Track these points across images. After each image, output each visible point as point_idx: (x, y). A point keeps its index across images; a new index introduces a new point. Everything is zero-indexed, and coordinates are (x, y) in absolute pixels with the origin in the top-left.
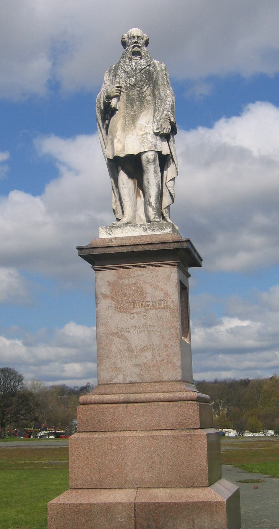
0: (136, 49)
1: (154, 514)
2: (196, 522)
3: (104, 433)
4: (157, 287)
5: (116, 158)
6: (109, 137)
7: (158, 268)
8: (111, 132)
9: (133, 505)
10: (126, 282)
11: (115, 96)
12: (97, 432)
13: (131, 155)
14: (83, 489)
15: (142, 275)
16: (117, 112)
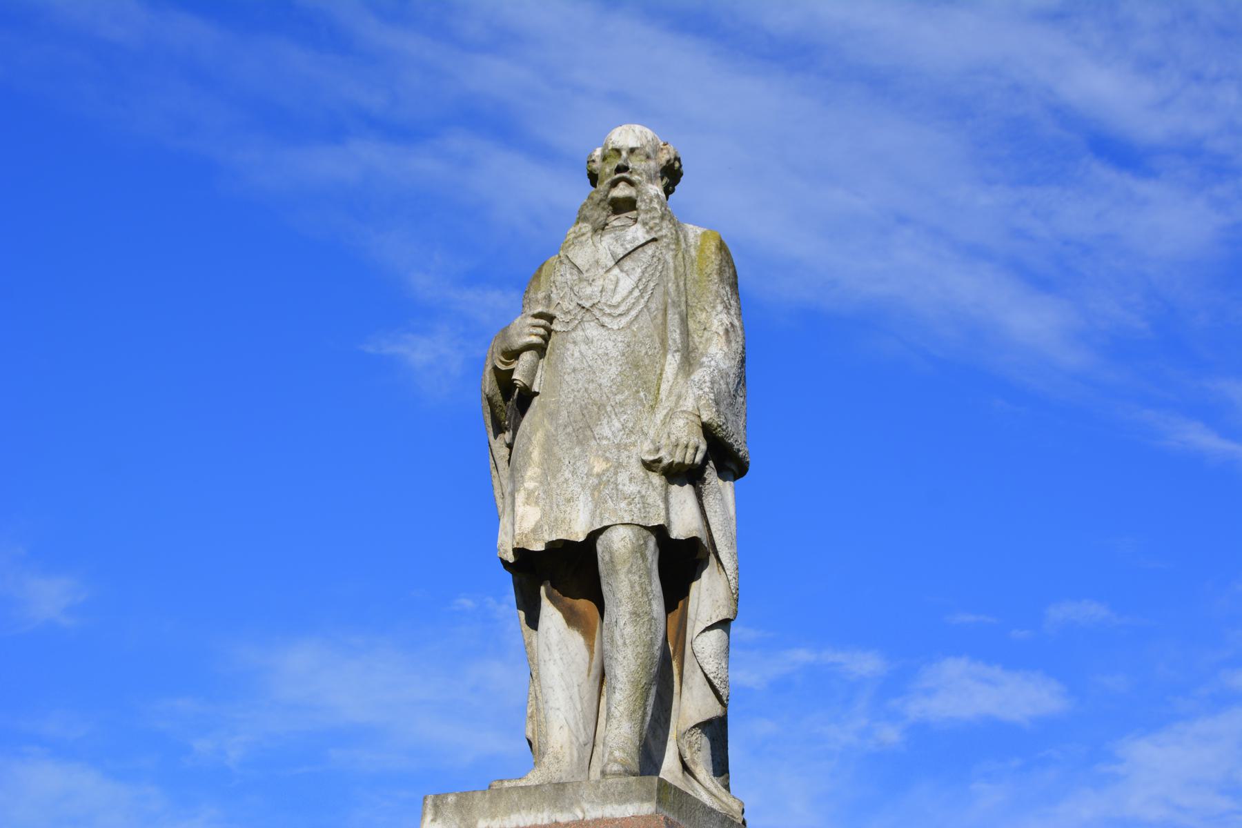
0: (622, 191)
13: (695, 575)
16: (536, 399)
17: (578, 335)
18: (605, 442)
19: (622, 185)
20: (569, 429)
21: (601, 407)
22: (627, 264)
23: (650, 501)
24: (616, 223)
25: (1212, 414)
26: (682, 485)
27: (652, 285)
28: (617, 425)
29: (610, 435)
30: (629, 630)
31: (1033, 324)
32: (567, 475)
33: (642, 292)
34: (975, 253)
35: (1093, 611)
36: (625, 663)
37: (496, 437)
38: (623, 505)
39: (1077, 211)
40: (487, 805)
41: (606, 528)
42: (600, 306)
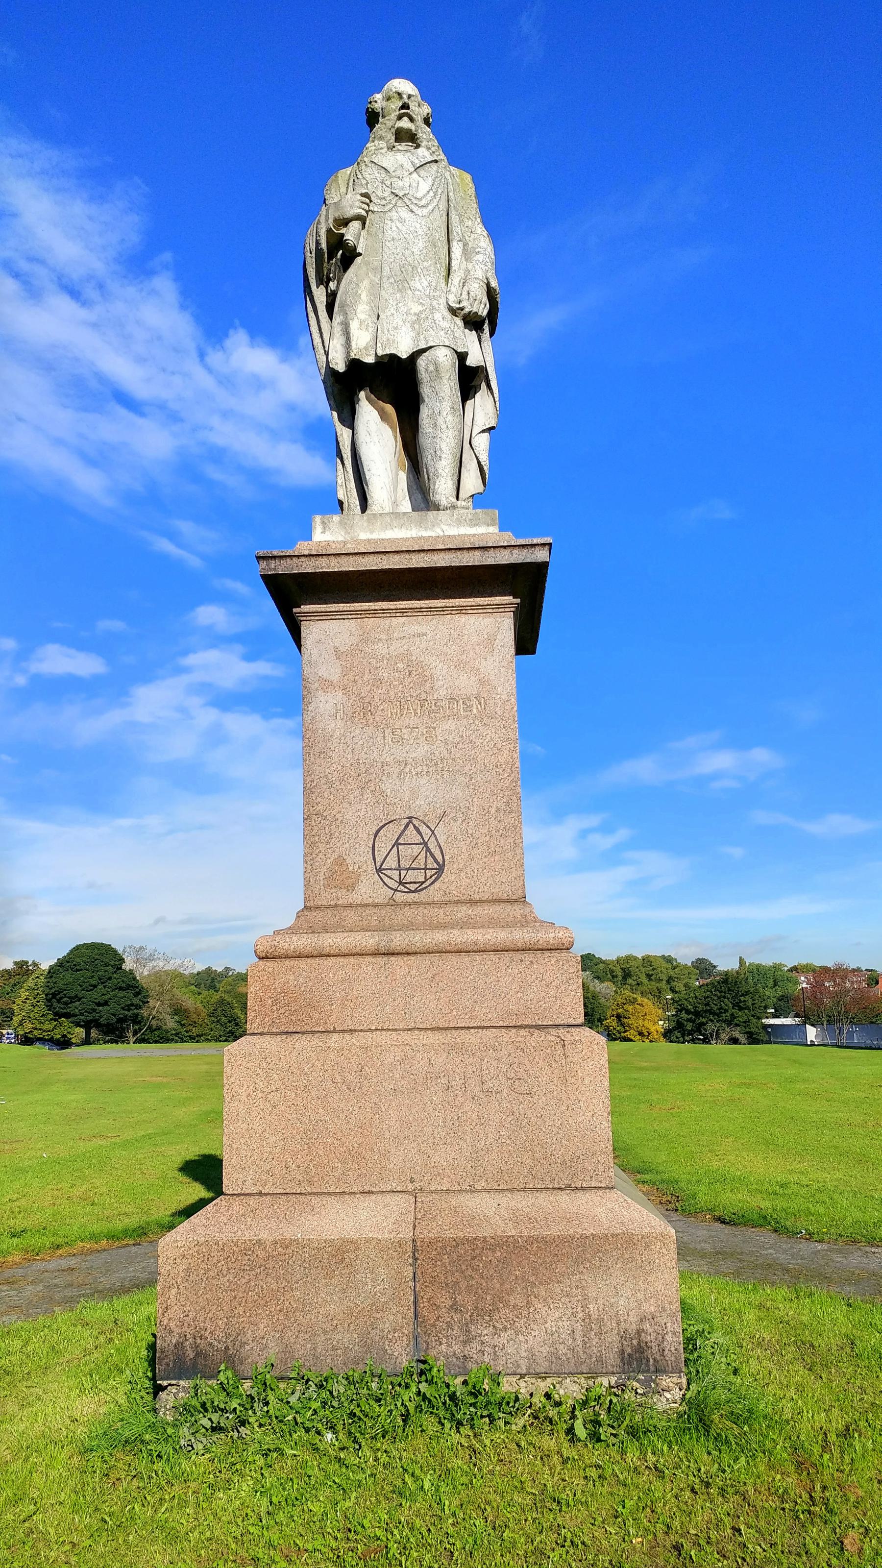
1: (469, 1272)
2: (592, 1294)
3: (324, 1036)
4: (460, 665)
5: (354, 365)
6: (338, 318)
7: (463, 618)
8: (342, 306)
9: (410, 1243)
10: (381, 649)
11: (358, 218)
12: (304, 1033)
14: (260, 1194)
15: (424, 635)
16: (358, 260)
17: (394, 214)
18: (417, 293)
19: (405, 119)
20: (392, 280)
21: (414, 268)
22: (422, 172)
23: (457, 335)
24: (400, 148)
25: (173, 536)
26: (471, 331)
27: (440, 191)
28: (426, 284)
29: (421, 288)
30: (450, 418)
31: (89, 483)
32: (392, 311)
33: (435, 193)
34: (59, 442)
35: (116, 625)
36: (448, 440)
37: (318, 287)
38: (442, 333)
39: (113, 427)
40: (365, 524)
41: (431, 347)
42: (409, 196)
